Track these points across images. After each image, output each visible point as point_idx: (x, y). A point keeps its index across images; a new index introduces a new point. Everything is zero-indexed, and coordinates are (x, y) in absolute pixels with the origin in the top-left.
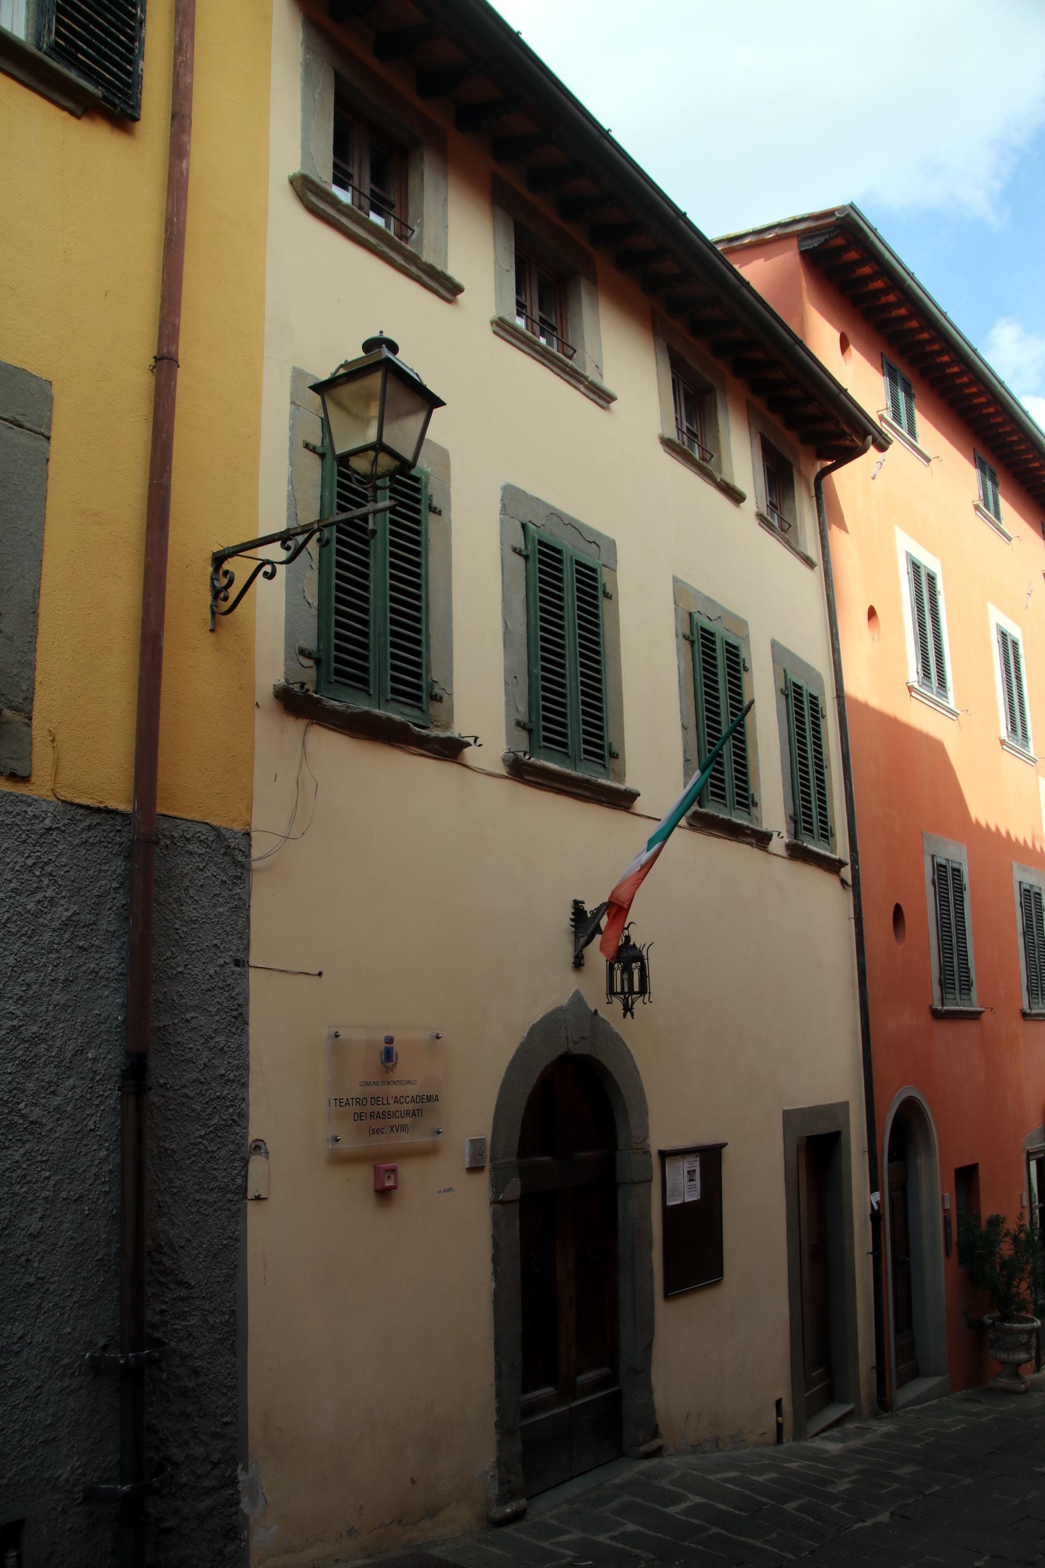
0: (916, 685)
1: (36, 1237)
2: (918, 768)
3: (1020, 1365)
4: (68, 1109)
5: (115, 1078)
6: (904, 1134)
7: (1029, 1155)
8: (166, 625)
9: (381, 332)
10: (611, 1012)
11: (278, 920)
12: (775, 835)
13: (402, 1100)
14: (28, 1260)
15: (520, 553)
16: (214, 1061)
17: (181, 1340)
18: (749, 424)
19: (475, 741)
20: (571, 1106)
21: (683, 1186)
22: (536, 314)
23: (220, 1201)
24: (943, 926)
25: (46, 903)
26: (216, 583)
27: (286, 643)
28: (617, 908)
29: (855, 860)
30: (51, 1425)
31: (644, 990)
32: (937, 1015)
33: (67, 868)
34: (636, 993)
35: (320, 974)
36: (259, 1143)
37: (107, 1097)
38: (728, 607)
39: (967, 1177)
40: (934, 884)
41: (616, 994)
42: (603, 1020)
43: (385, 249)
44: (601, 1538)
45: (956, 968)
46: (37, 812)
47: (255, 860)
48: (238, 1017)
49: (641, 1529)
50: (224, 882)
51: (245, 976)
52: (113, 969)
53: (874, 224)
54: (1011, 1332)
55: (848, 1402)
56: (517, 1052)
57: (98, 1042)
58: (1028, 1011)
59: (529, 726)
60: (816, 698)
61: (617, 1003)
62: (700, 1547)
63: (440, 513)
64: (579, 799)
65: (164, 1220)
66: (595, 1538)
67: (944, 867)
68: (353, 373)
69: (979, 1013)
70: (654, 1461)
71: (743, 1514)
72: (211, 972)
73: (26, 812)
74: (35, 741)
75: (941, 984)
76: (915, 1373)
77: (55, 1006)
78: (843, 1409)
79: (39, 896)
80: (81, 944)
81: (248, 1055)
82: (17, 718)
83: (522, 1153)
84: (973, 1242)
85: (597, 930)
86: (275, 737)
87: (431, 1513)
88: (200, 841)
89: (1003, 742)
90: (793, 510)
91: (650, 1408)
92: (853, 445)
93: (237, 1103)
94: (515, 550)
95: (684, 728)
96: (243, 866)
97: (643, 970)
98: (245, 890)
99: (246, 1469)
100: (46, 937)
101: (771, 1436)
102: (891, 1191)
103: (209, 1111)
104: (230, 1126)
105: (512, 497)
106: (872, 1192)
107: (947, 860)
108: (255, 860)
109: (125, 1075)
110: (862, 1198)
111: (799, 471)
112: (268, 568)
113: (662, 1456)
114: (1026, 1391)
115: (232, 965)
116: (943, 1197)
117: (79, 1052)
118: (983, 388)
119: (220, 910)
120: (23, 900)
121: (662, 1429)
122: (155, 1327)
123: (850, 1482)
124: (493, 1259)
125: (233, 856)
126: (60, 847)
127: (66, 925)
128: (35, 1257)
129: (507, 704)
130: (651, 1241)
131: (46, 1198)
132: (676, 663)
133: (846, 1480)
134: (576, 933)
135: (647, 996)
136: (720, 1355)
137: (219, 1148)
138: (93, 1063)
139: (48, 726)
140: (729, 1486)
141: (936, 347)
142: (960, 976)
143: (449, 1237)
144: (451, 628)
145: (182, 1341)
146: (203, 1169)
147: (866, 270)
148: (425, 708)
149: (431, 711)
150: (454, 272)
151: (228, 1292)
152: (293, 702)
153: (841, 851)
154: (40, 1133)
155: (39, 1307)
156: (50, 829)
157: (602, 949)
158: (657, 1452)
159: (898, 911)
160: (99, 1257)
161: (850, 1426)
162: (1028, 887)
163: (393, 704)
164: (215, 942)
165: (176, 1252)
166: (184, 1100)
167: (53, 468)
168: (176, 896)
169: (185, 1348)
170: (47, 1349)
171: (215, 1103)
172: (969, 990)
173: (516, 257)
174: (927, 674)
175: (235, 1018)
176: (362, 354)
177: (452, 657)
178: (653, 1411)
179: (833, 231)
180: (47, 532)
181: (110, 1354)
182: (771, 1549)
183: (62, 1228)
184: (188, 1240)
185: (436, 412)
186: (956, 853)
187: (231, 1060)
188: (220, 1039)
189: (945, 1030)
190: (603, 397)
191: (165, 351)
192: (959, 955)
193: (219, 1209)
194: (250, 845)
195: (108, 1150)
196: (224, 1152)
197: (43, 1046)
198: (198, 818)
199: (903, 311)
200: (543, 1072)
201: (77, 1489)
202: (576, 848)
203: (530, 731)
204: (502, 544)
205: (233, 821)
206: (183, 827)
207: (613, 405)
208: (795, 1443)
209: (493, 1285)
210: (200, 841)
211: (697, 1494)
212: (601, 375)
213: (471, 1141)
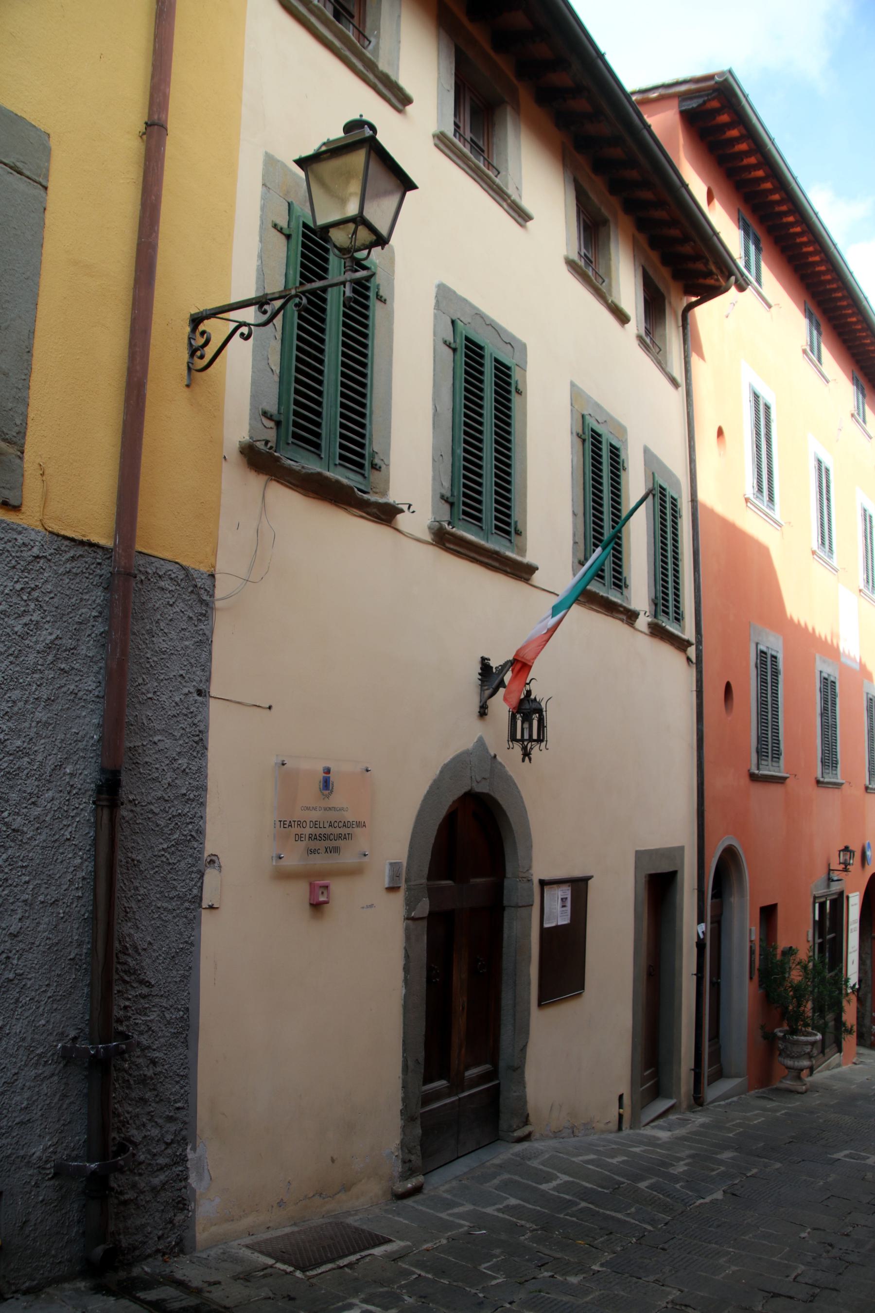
0: (751, 497)
1: (15, 936)
2: (749, 566)
3: (802, 1070)
4: (47, 819)
5: (90, 793)
6: (724, 875)
7: (815, 898)
8: (149, 376)
9: (361, 116)
10: (509, 757)
11: (235, 657)
12: (642, 614)
13: (336, 824)
14: (8, 958)
15: (449, 346)
16: (177, 781)
17: (141, 1033)
18: (634, 256)
19: (409, 508)
20: (471, 838)
21: (558, 914)
22: (468, 135)
23: (179, 909)
24: (762, 704)
25: (32, 627)
26: (193, 341)
27: (251, 404)
28: (521, 665)
29: (699, 642)
30: (26, 1108)
32: (754, 778)
33: (52, 595)
34: (535, 741)
35: (270, 708)
36: (213, 858)
37: (82, 810)
38: (612, 413)
39: (768, 913)
40: (757, 667)
41: (518, 741)
42: (500, 764)
43: (348, 53)
44: (490, 1210)
45: (770, 740)
46: (26, 541)
47: (218, 600)
48: (198, 742)
49: (522, 1203)
50: (190, 618)
51: (206, 705)
52: (90, 692)
53: (747, 90)
54: (797, 1043)
55: (671, 1097)
56: (431, 787)
57: (75, 758)
58: (822, 779)
59: (451, 500)
60: (675, 500)
61: (517, 748)
62: (574, 1219)
63: (385, 302)
65: (129, 924)
66: (484, 1210)
67: (765, 653)
68: (333, 151)
69: (785, 778)
70: (525, 1145)
71: (605, 1191)
72: (177, 699)
73: (16, 539)
74: (26, 474)
75: (758, 752)
76: (719, 1075)
77: (38, 723)
78: (670, 1102)
79: (26, 619)
80: (63, 666)
81: (206, 777)
82: (11, 450)
83: (429, 878)
84: (770, 970)
85: (501, 684)
86: (240, 487)
87: (346, 1188)
88: (171, 579)
89: (814, 553)
90: (663, 337)
92: (717, 284)
93: (196, 820)
94: (445, 342)
95: (574, 514)
96: (207, 605)
97: (541, 721)
98: (208, 627)
99: (194, 1149)
100: (32, 658)
101: (614, 1125)
102: (712, 923)
103: (171, 826)
104: (189, 841)
105: (445, 296)
106: (699, 923)
107: (768, 648)
108: (218, 600)
109: (99, 790)
110: (691, 928)
111: (670, 303)
112: (245, 330)
113: (530, 1140)
114: (806, 1092)
115: (195, 695)
116: (750, 930)
117: (59, 767)
118: (818, 248)
119: (187, 643)
120: (11, 622)
121: (532, 1118)
122: (119, 1021)
123: (686, 1165)
124: (404, 968)
125: (198, 594)
126: (46, 574)
127: (50, 648)
128: (15, 954)
129: (434, 479)
130: (530, 957)
131: (25, 901)
132: (570, 457)
133: (682, 1163)
134: (482, 686)
135: (543, 744)
136: (575, 1056)
137: (179, 861)
138: (70, 778)
139: (38, 460)
140: (590, 1167)
141: (784, 208)
142: (773, 746)
143: (370, 949)
144: (390, 405)
145: (142, 1034)
146: (164, 878)
147: (734, 133)
148: (366, 475)
149: (372, 478)
150: (405, 82)
151: (183, 991)
152: (257, 459)
153: (688, 633)
154: (21, 841)
155: (17, 1001)
156: (37, 557)
157: (505, 699)
158: (527, 1138)
159: (728, 688)
160: (71, 957)
161: (672, 1117)
162: (826, 676)
163: (340, 469)
164: (181, 672)
165: (139, 954)
166: (150, 816)
167: (49, 217)
168: (148, 628)
169: (144, 1040)
170: (23, 1039)
171: (177, 819)
172: (779, 758)
173: (456, 75)
174: (760, 490)
175: (196, 742)
176: (342, 134)
177: (390, 432)
178: (525, 1102)
179: (711, 94)
180: (42, 277)
181: (82, 1045)
182: (633, 1221)
183: (39, 929)
184: (150, 943)
185: (409, 194)
186: (773, 643)
187: (191, 781)
188: (183, 762)
189: (759, 791)
190: (521, 216)
191: (156, 117)
192: (772, 729)
193: (178, 916)
194: (214, 586)
195: (82, 858)
196: (183, 864)
197: (26, 759)
198: (170, 558)
199: (760, 173)
200: (451, 806)
201: (48, 1166)
202: (487, 614)
203: (452, 505)
204: (435, 335)
205: (201, 563)
206: (157, 564)
207: (529, 224)
208: (632, 1131)
209: (404, 991)
210: (171, 579)
211: (565, 1173)
212: (520, 197)
213: (391, 864)
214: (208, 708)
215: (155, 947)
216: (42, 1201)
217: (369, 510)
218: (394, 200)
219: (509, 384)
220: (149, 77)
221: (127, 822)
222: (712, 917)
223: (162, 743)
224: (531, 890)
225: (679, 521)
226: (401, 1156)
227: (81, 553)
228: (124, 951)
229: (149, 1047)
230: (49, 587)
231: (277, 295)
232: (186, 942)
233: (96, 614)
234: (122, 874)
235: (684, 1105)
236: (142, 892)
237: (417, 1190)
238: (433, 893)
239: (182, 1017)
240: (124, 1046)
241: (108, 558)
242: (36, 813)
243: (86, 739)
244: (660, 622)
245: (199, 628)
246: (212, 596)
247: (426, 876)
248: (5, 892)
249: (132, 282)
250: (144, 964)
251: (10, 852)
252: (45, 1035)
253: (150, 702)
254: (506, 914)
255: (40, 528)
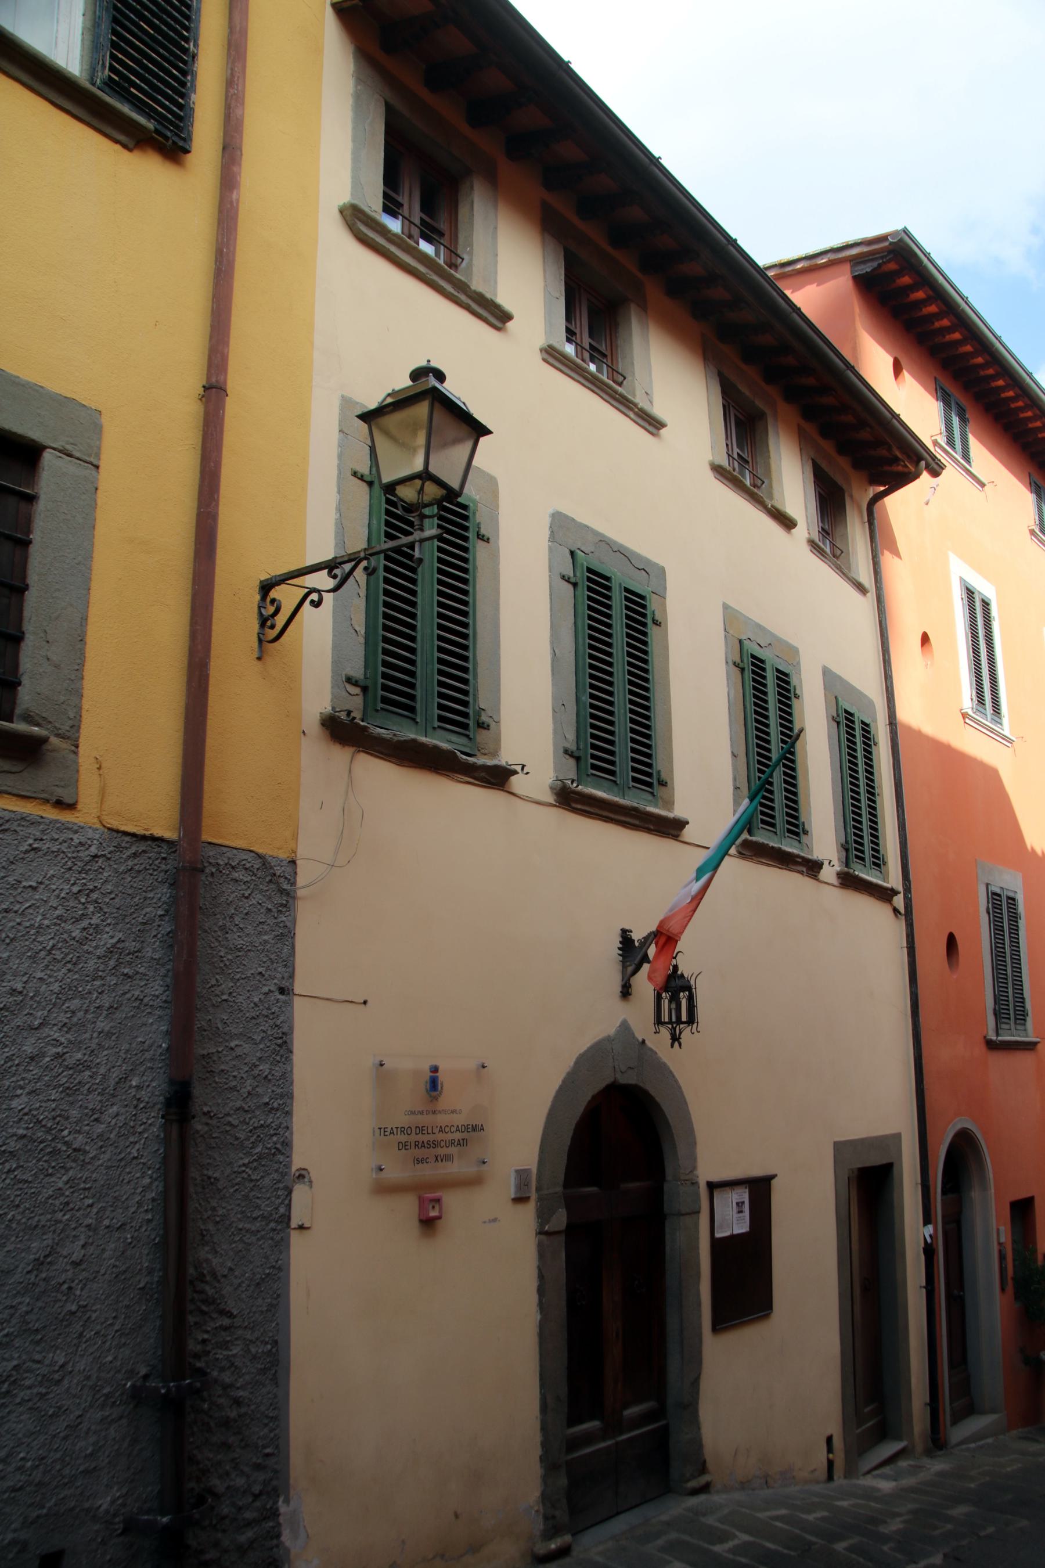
0: (970, 712)
2: (974, 792)
4: (112, 1136)
5: (159, 1106)
6: (959, 1165)
9: (429, 361)
10: (659, 1042)
11: (324, 948)
12: (826, 863)
14: (70, 1288)
17: (222, 1370)
20: (617, 1140)
21: (733, 1220)
25: (91, 931)
26: (263, 610)
27: (333, 671)
28: (666, 938)
29: (907, 889)
30: (91, 1454)
32: (992, 1046)
33: (113, 896)
35: (365, 1002)
36: (303, 1172)
37: (150, 1125)
40: (988, 913)
42: (651, 1050)
43: (435, 277)
45: (1011, 998)
50: (269, 910)
51: (289, 1004)
52: (158, 997)
55: (899, 1438)
57: (142, 1069)
59: (576, 754)
61: (665, 1033)
63: (488, 541)
65: (207, 1248)
67: (999, 895)
68: (400, 402)
69: (1035, 1044)
70: (702, 1498)
71: (792, 1553)
72: (256, 1000)
74: (81, 769)
75: (995, 1014)
76: (969, 1410)
77: (100, 1033)
79: (85, 923)
80: (126, 971)
83: (566, 1185)
85: (645, 959)
86: (323, 764)
88: (246, 869)
90: (845, 537)
91: (697, 1444)
92: (906, 470)
93: (281, 1131)
94: (563, 577)
95: (734, 755)
96: (288, 894)
97: (691, 999)
99: (287, 1501)
100: (91, 964)
101: (822, 1473)
102: (944, 1223)
103: (252, 1139)
104: (274, 1154)
107: (1002, 888)
109: (168, 1103)
110: (915, 1231)
111: (851, 496)
112: (314, 597)
115: (277, 993)
116: (998, 1230)
117: (124, 1079)
119: (266, 937)
121: (710, 1465)
122: (197, 1356)
126: (106, 874)
127: (111, 952)
129: (555, 732)
131: (88, 1226)
132: (726, 690)
134: (623, 962)
136: (768, 1390)
142: (1015, 1006)
150: (504, 299)
152: (340, 730)
153: (894, 879)
156: (96, 856)
157: (650, 978)
158: (705, 1489)
161: (903, 1464)
164: (260, 970)
165: (219, 1281)
166: (228, 1128)
168: (221, 924)
169: (227, 1377)
170: (88, 1378)
171: (259, 1132)
172: (1025, 1020)
175: (279, 1046)
177: (499, 685)
178: (700, 1446)
179: (885, 256)
180: (95, 560)
181: (152, 1384)
187: (274, 1088)
188: (265, 1067)
189: (999, 1061)
190: (652, 424)
193: (262, 1237)
194: (296, 873)
195: (151, 1177)
196: (267, 1181)
197: (88, 1073)
198: (244, 846)
200: (590, 1102)
201: (117, 1520)
202: (627, 878)
203: (578, 759)
204: (550, 571)
207: (663, 431)
209: (539, 1317)
210: (246, 869)
211: (745, 1532)
212: (651, 402)
213: (517, 1171)
214: (292, 1007)
215: (236, 1273)
216: (110, 1561)
217: (476, 774)
218: (469, 445)
219: (644, 616)
220: (208, 337)
221: (202, 1136)
222: (943, 1217)
223: (240, 1049)
224: (698, 1195)
225: (874, 749)
226: (542, 1511)
227: (144, 848)
228: (201, 1277)
229: (231, 1386)
230: (109, 887)
231: (346, 559)
232: (273, 1267)
233: (162, 913)
234: (196, 1193)
235: (919, 1447)
236: (220, 1213)
237: (564, 1552)
238: (570, 1203)
239: (270, 1351)
240: (198, 1385)
241: (175, 852)
242: (100, 1130)
243: (153, 1048)
244: (851, 871)
245: (280, 920)
246: (294, 884)
247: (561, 1183)
248: (66, 1217)
249: (192, 555)
250: (224, 1292)
251: (71, 1173)
252: (112, 1373)
253: (225, 1004)
254: (667, 1224)
255: (98, 826)
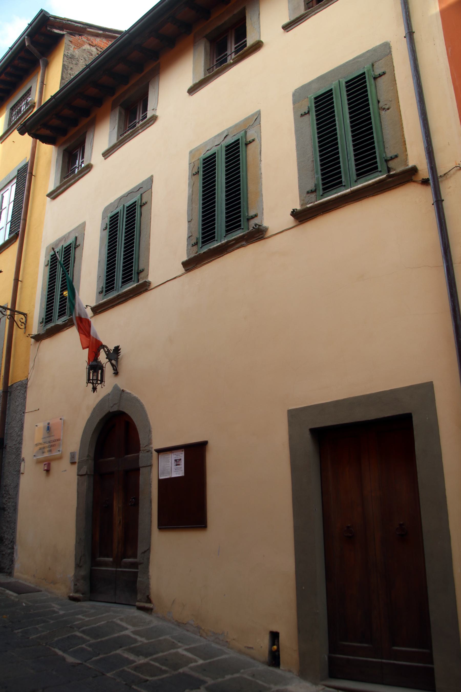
21: (172, 468)
31: (102, 381)
42: (127, 393)
43: (69, 184)
64: (113, 307)
91: (148, 587)
